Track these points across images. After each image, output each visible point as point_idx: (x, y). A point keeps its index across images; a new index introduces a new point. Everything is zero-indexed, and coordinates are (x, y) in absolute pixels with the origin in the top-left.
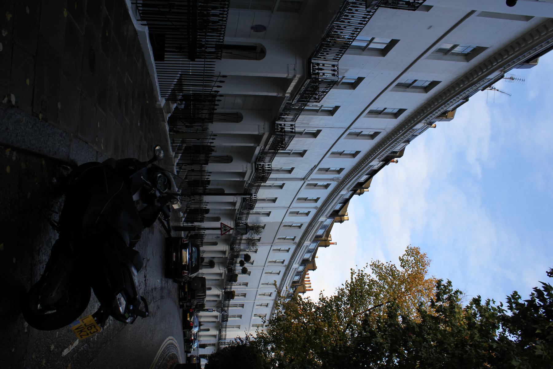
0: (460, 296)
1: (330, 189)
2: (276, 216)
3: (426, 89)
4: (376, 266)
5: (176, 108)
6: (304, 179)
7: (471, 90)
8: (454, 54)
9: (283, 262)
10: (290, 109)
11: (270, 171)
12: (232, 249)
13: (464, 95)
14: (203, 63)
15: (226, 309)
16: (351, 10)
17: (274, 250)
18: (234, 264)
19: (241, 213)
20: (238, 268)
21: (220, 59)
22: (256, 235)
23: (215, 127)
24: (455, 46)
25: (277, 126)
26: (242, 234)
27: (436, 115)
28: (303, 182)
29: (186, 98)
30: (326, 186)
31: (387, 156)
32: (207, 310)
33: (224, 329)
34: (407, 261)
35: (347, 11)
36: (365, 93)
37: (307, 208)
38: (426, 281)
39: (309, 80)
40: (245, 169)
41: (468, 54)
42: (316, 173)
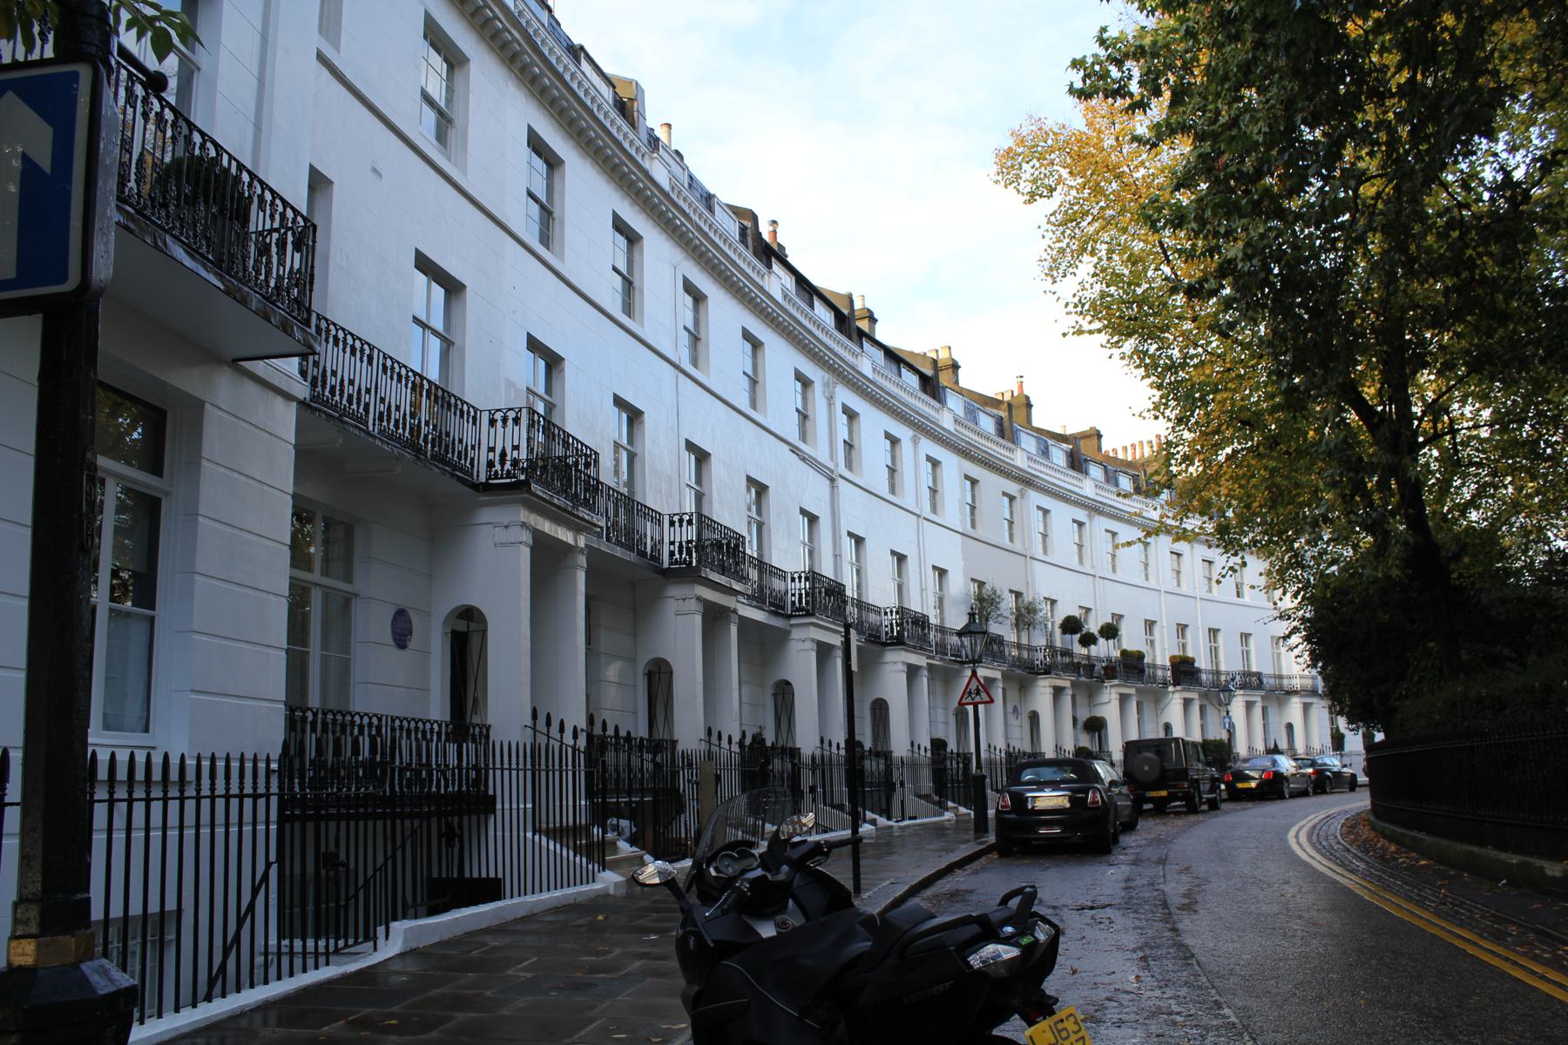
0: (1113, 33)
1: (857, 403)
2: (947, 550)
3: (554, 164)
4: (1056, 268)
5: (632, 841)
6: (832, 480)
7: (550, 42)
8: (449, 100)
9: (1080, 524)
10: (630, 531)
11: (813, 576)
12: (1047, 671)
13: (566, 59)
14: (506, 773)
15: (1223, 678)
16: (333, 388)
17: (1045, 552)
18: (1090, 660)
19: (942, 648)
20: (1104, 649)
21: (488, 729)
22: (1003, 605)
23: (688, 732)
24: (427, 98)
25: (676, 562)
26: (981, 646)
27: (625, 128)
28: (840, 481)
29: (600, 814)
30: (851, 415)
31: (755, 254)
32: (1231, 733)
33: (1285, 682)
34: (1034, 181)
35: (337, 398)
36: (652, 387)
37: (916, 466)
38: (1090, 124)
39: (534, 486)
40: (809, 645)
41: (446, 60)
42: (815, 445)
